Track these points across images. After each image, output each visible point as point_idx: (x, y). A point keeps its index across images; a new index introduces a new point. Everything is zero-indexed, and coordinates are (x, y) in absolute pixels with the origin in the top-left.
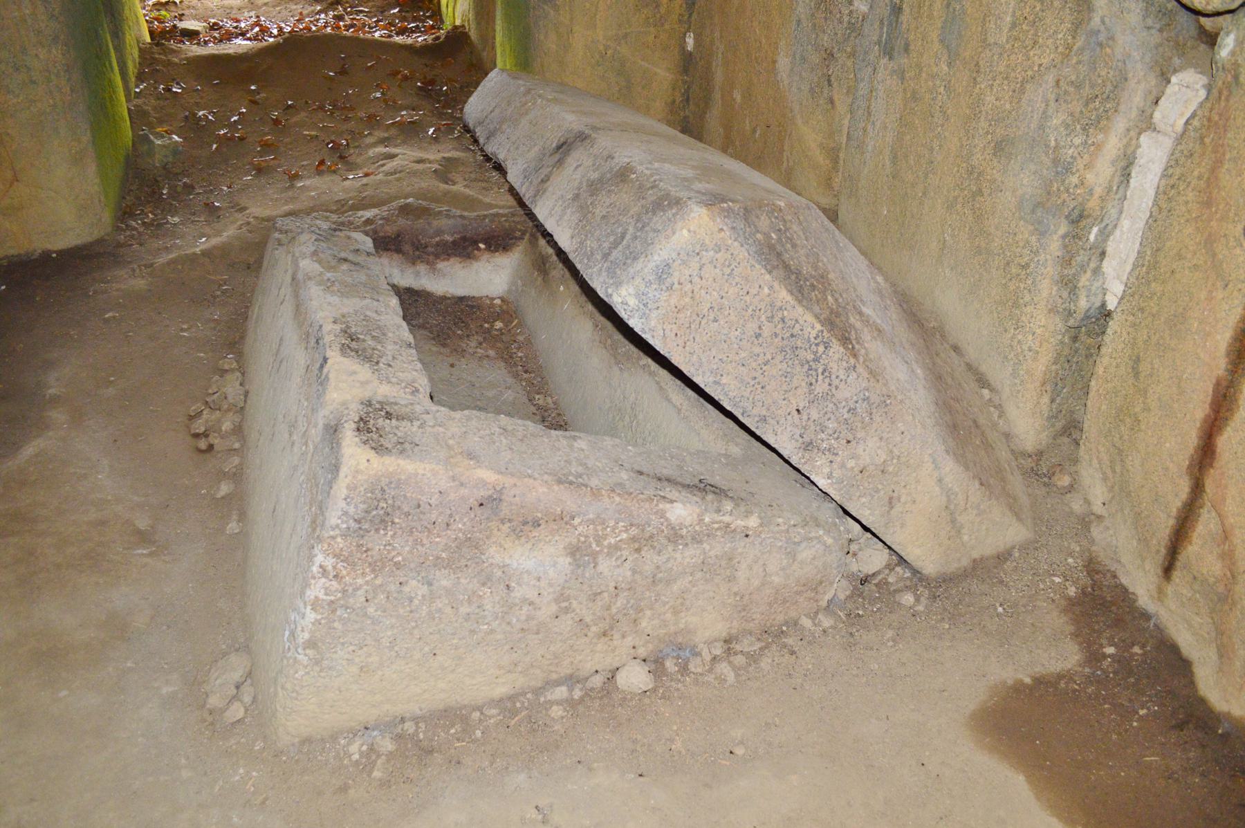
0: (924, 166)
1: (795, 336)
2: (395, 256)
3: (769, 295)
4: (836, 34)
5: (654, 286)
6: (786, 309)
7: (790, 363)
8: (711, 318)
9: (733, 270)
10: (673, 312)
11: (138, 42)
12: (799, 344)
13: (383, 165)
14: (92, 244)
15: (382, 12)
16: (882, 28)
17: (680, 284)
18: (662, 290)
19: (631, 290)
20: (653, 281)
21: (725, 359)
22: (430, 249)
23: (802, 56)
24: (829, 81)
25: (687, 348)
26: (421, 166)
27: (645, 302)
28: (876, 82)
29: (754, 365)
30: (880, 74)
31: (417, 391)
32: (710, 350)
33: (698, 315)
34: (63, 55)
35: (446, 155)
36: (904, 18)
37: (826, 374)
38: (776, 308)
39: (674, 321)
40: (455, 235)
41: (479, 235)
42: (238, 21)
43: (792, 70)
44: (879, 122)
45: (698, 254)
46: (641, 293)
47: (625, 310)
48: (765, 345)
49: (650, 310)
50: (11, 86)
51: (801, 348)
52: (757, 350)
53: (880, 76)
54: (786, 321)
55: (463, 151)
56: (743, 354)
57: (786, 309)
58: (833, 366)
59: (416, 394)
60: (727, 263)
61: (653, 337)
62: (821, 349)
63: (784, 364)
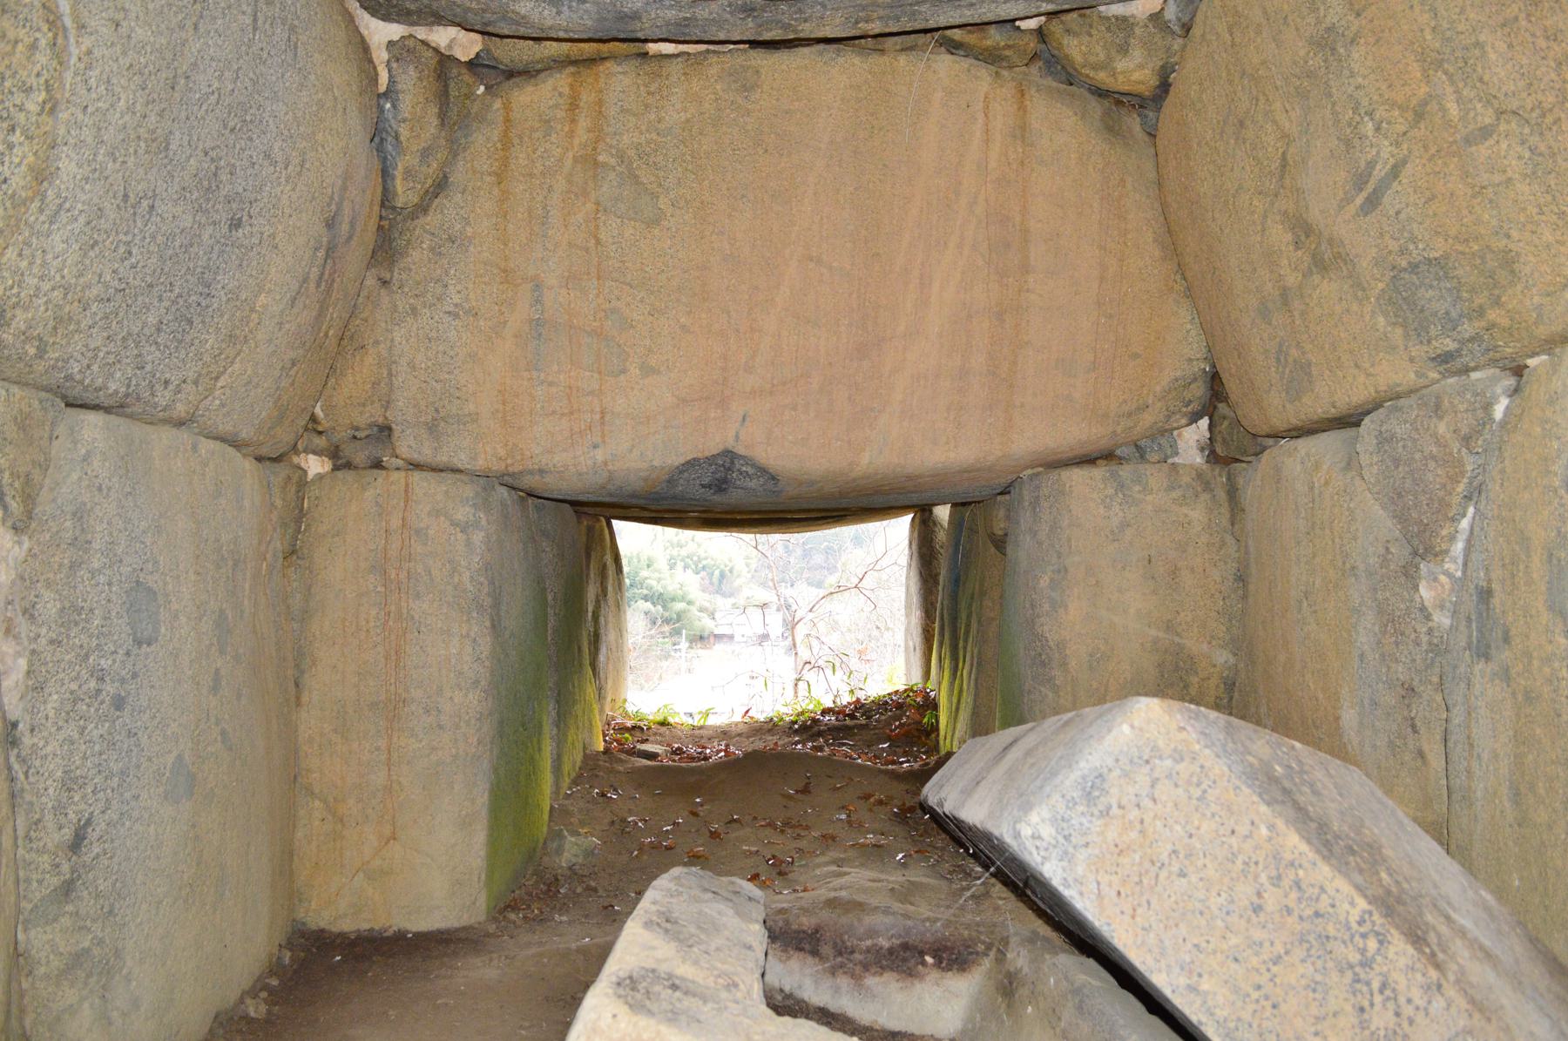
0: (1561, 791)
1: (1322, 916)
2: (810, 960)
3: (1270, 839)
4: (1414, 661)
5: (1081, 808)
6: (1300, 866)
7: (1319, 964)
8: (1175, 868)
9: (1205, 792)
10: (1112, 854)
11: (585, 748)
12: (1331, 930)
13: (829, 882)
14: (457, 930)
15: (869, 746)
16: (1469, 627)
17: (1120, 807)
18: (1092, 815)
19: (1046, 814)
20: (1078, 800)
21: (1204, 945)
22: (858, 956)
23: (1372, 700)
24: (1413, 726)
25: (1138, 919)
26: (875, 884)
27: (1066, 833)
28: (1473, 698)
29: (1255, 961)
30: (1477, 686)
31: (736, 985)
32: (1177, 925)
33: (1153, 863)
34: (480, 702)
35: (912, 879)
36: (1496, 601)
37: (1388, 992)
38: (1284, 863)
39: (1114, 868)
40: (894, 940)
41: (926, 943)
42: (705, 748)
43: (1361, 723)
44: (1486, 751)
45: (1147, 762)
46: (1059, 817)
47: (1037, 848)
48: (1270, 926)
49: (1075, 847)
50: (416, 729)
51: (1336, 939)
52: (1258, 935)
53: (1477, 689)
54: (1304, 886)
55: (936, 878)
56: (1234, 940)
57: (1300, 866)
58: (1400, 980)
59: (732, 989)
60: (1195, 780)
61: (1081, 894)
62: (1372, 944)
63: (1308, 964)
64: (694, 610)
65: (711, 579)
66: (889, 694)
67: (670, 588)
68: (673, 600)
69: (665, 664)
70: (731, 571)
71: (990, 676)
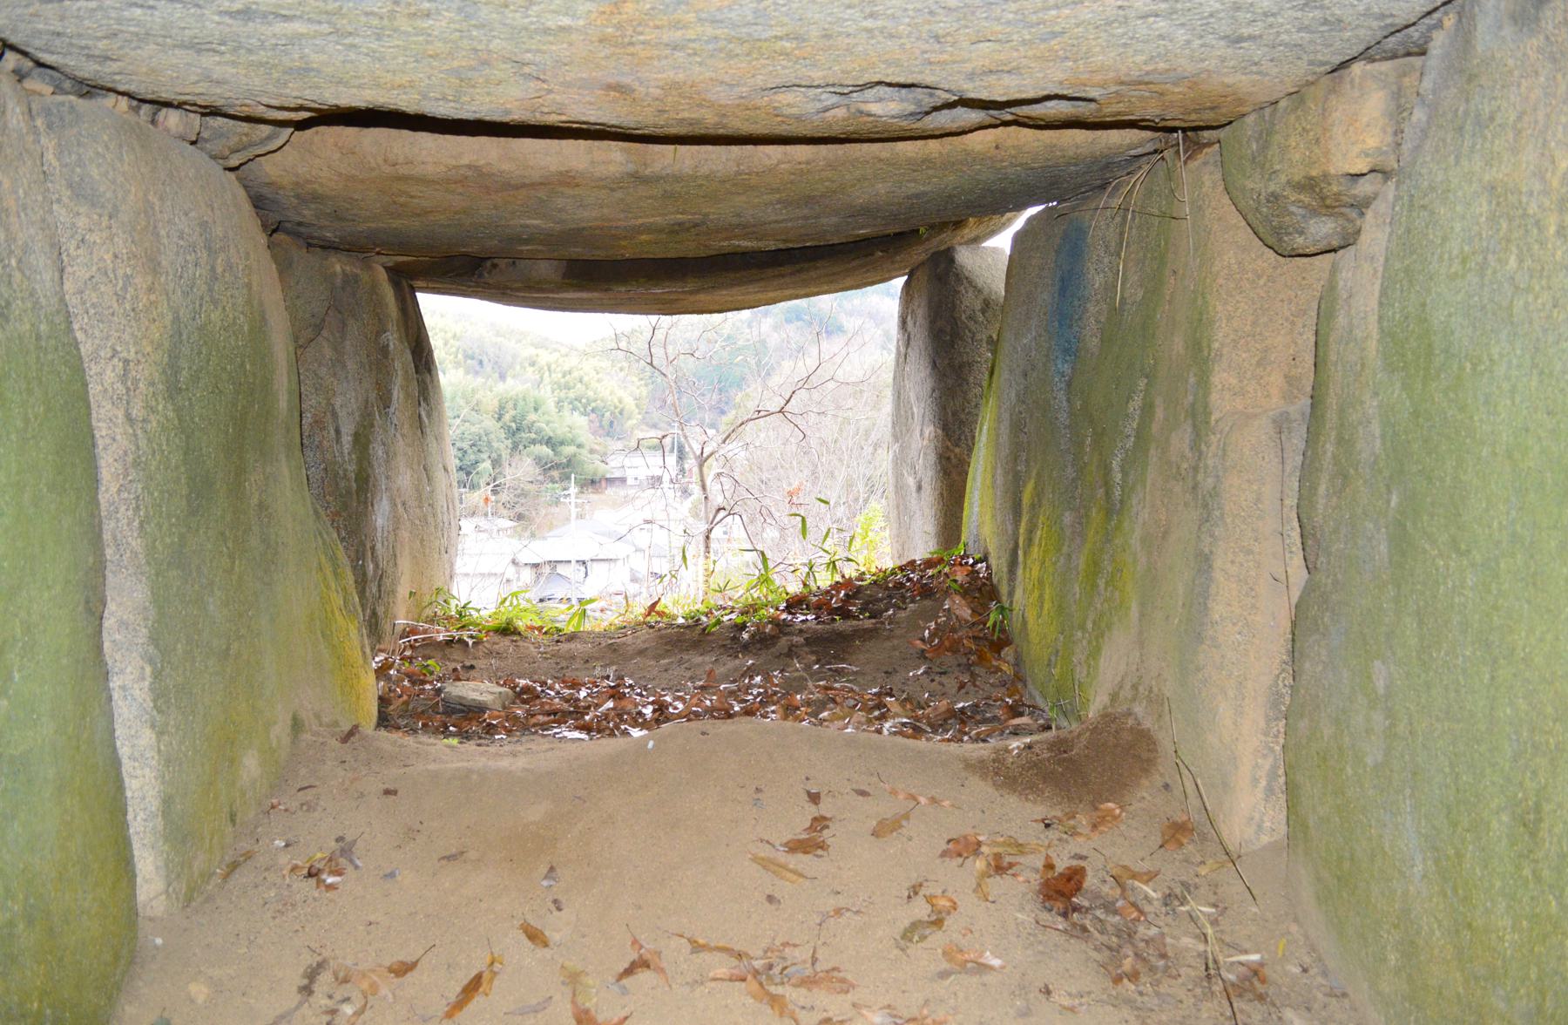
42: (575, 685)
64: (584, 452)
65: (601, 422)
66: (901, 569)
67: (559, 432)
68: (562, 443)
69: (555, 510)
70: (621, 413)
71: (1249, 552)
